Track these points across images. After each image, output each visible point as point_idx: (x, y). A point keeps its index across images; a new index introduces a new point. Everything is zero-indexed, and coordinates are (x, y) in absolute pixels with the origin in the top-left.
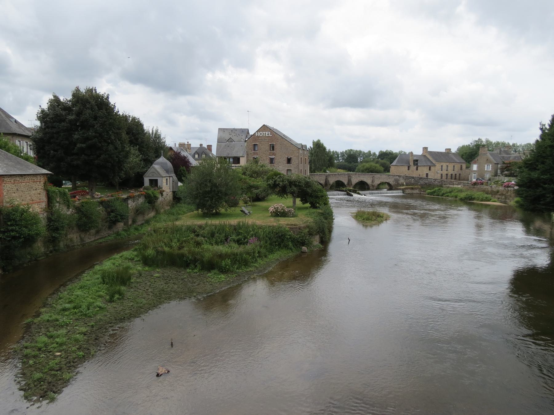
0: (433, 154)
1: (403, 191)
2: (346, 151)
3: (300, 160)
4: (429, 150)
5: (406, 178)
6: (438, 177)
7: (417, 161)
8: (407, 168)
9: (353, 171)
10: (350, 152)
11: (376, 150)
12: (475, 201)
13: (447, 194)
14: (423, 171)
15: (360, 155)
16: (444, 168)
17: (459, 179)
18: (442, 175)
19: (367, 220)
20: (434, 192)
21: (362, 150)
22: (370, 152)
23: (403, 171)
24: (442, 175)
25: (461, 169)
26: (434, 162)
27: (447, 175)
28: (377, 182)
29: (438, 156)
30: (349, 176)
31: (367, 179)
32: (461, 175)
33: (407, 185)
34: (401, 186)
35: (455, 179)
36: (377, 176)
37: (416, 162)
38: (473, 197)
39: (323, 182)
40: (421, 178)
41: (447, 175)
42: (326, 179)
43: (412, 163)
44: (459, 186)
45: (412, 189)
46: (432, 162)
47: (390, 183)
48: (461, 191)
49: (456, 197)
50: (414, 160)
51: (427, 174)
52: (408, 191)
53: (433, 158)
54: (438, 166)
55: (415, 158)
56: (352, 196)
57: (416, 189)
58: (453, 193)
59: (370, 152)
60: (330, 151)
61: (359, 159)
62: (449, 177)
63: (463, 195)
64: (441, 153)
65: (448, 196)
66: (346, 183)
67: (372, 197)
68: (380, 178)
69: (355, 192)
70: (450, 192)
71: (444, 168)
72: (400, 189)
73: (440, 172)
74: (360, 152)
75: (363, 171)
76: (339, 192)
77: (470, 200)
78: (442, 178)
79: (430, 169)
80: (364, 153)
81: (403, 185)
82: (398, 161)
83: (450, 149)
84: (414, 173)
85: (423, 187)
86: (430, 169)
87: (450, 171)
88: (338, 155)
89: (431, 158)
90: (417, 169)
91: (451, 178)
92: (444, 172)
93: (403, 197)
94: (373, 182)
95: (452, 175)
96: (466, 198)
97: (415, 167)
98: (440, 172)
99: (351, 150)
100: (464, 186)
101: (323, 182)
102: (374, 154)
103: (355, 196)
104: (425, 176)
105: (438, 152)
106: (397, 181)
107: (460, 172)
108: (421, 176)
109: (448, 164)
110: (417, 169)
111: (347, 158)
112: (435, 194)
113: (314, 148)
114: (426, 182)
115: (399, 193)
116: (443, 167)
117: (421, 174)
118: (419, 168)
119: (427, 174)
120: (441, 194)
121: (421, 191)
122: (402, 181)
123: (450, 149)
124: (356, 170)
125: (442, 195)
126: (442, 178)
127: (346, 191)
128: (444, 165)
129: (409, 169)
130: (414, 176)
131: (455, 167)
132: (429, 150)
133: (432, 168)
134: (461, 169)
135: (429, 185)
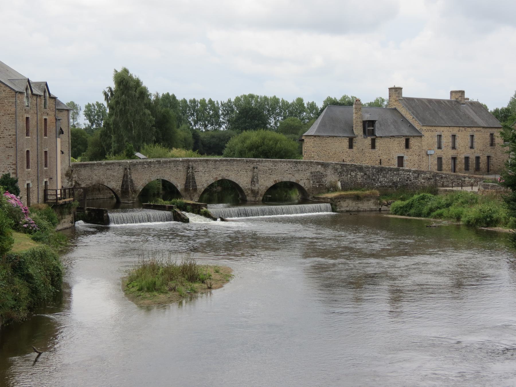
0: (413, 103)
1: (334, 204)
2: (238, 99)
3: (22, 123)
4: (405, 94)
5: (344, 168)
6: (431, 165)
7: (372, 123)
8: (346, 143)
9: (220, 154)
10: (249, 103)
11: (223, 91)
12: (499, 229)
13: (439, 211)
14: (388, 151)
15: (274, 109)
16: (446, 141)
17: (488, 171)
18: (440, 159)
19: (149, 290)
20: (410, 206)
21: (280, 97)
22: (300, 101)
23: (337, 150)
24: (440, 159)
25: (492, 144)
26: (417, 125)
27: (454, 159)
28: (266, 182)
29: (429, 111)
30: (189, 166)
31: (240, 174)
32: (493, 161)
33: (345, 188)
34: (328, 190)
35: (478, 169)
36: (266, 164)
37: (369, 127)
38: (495, 216)
39: (115, 184)
40: (381, 170)
41: (454, 159)
42: (125, 176)
43: (358, 131)
44: (475, 189)
45: (357, 198)
46: (411, 126)
47: (301, 183)
48: (471, 201)
49: (458, 218)
50: (364, 122)
51: (401, 159)
52: (346, 205)
53: (416, 115)
54: (429, 136)
55: (367, 117)
56: (187, 221)
57: (367, 198)
58: (451, 208)
59: (300, 101)
60: (185, 101)
61: (272, 121)
62: (461, 165)
63: (471, 213)
64: (439, 102)
65: (440, 216)
66: (180, 186)
67: (240, 224)
68: (273, 172)
69: (196, 210)
70: (448, 205)
71: (446, 141)
72: (325, 200)
73: (434, 152)
74: (276, 100)
75: (241, 154)
76: (152, 213)
77: (488, 224)
78: (440, 168)
79: (407, 146)
80: (286, 106)
81: (335, 189)
82: (323, 125)
83: (463, 92)
84: (364, 155)
85: (386, 192)
86: (407, 146)
87: (463, 150)
88: (93, 105)
89: (409, 117)
90: (373, 146)
91: (467, 168)
92: (447, 153)
93: (331, 222)
94: (253, 181)
95: (467, 159)
96: (478, 221)
97: (368, 141)
98: (434, 152)
99: (252, 96)
100: (486, 187)
101: (115, 184)
102: (312, 106)
103: (196, 220)
104: (394, 164)
105: (430, 101)
106: (318, 177)
107: (489, 151)
108: (384, 165)
109: (455, 131)
110: (373, 146)
111: (238, 118)
112: (412, 211)
113: (116, 91)
114: (395, 179)
115: (323, 211)
116: (444, 141)
117: (384, 157)
118: (378, 143)
119: (401, 159)
120: (425, 210)
121: (381, 204)
122: (331, 178)
123: (463, 92)
124: (225, 152)
125: (428, 214)
126: (440, 168)
127: (170, 209)
128: (446, 134)
129: (351, 146)
130: (366, 163)
131: (476, 139)
132: (405, 94)
133: (412, 141)
134: (492, 144)
135: (403, 188)
